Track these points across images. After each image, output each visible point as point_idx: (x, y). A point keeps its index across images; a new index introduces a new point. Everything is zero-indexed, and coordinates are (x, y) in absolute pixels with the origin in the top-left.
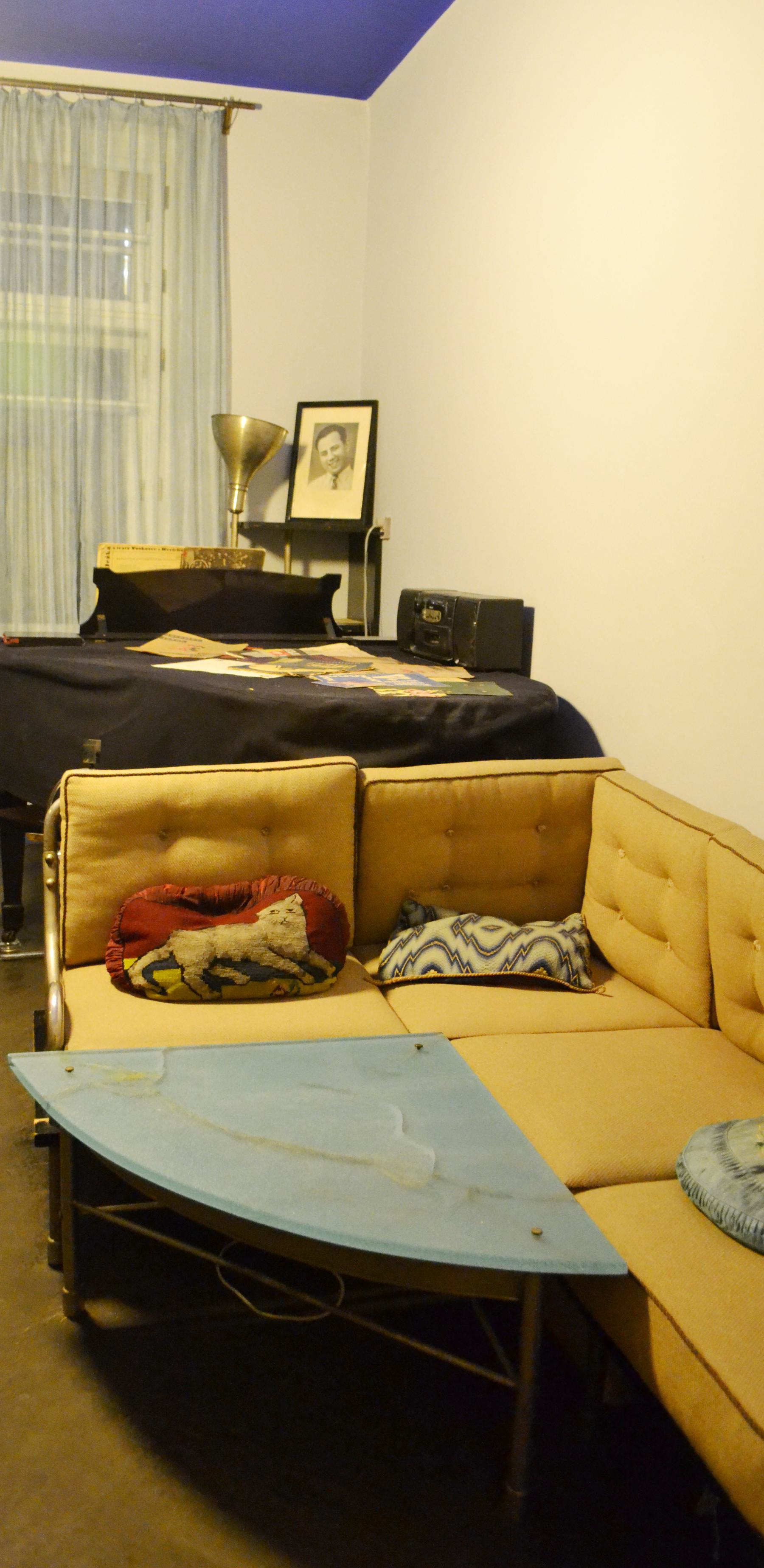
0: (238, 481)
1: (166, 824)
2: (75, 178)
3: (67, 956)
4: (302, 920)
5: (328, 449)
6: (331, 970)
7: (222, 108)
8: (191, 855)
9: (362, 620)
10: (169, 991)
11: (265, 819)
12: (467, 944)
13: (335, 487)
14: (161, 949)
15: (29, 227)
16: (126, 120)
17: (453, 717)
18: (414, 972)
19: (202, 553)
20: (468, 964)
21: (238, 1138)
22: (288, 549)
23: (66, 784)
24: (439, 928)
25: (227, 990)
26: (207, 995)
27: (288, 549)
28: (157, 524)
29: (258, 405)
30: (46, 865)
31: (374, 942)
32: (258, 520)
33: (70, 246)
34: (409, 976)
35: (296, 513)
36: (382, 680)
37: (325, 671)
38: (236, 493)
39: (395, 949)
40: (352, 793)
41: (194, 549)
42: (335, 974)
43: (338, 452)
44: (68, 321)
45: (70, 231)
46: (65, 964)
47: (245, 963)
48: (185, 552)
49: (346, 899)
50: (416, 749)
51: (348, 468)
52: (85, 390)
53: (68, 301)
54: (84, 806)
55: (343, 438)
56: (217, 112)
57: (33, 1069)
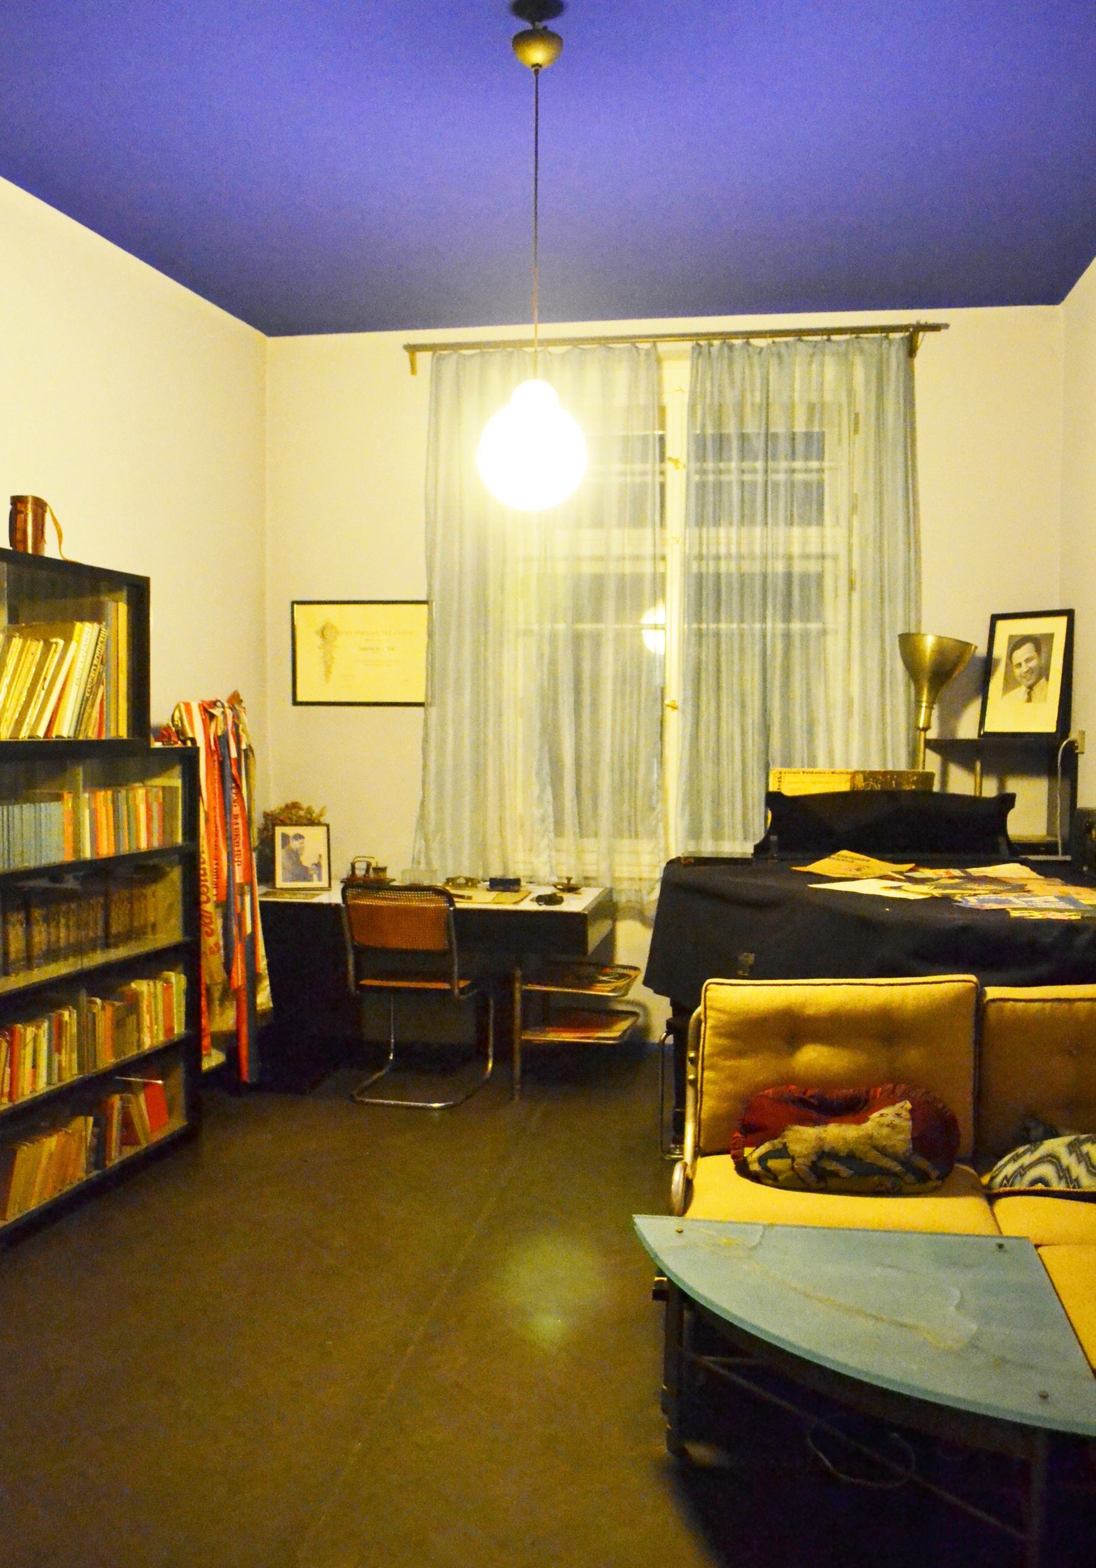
0: (925, 698)
1: (791, 1029)
2: (764, 415)
3: (701, 1145)
4: (907, 1124)
5: (1022, 660)
6: (934, 1174)
7: (907, 334)
8: (813, 1058)
9: (1056, 836)
10: (780, 1178)
11: (881, 1029)
12: (1080, 1162)
13: (1029, 700)
14: (776, 1141)
15: (722, 465)
16: (812, 355)
17: (1082, 940)
18: (1022, 1184)
19: (870, 776)
20: (1077, 1180)
21: (806, 1296)
22: (978, 765)
23: (706, 991)
24: (1056, 1145)
25: (832, 1182)
26: (814, 1185)
27: (978, 765)
28: (847, 742)
29: (949, 619)
30: (689, 1063)
31: (986, 1156)
32: (949, 737)
33: (760, 478)
34: (1016, 1188)
35: (989, 727)
36: (1026, 902)
37: (973, 892)
38: (923, 710)
39: (1009, 1162)
40: (972, 1008)
41: (863, 772)
42: (938, 1178)
43: (1033, 663)
44: (757, 550)
45: (759, 465)
46: (700, 1152)
47: (850, 1158)
48: (854, 774)
49: (963, 1109)
50: (1043, 969)
51: (1043, 680)
52: (774, 615)
53: (758, 530)
54: (719, 1011)
55: (1038, 650)
56: (902, 338)
57: (653, 1229)
